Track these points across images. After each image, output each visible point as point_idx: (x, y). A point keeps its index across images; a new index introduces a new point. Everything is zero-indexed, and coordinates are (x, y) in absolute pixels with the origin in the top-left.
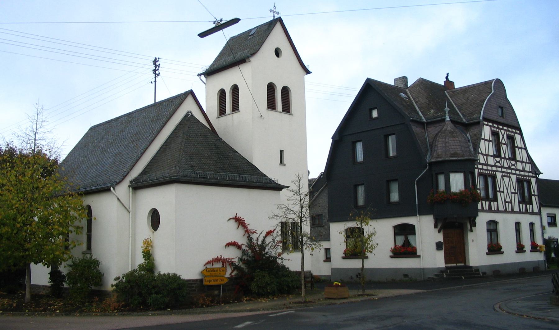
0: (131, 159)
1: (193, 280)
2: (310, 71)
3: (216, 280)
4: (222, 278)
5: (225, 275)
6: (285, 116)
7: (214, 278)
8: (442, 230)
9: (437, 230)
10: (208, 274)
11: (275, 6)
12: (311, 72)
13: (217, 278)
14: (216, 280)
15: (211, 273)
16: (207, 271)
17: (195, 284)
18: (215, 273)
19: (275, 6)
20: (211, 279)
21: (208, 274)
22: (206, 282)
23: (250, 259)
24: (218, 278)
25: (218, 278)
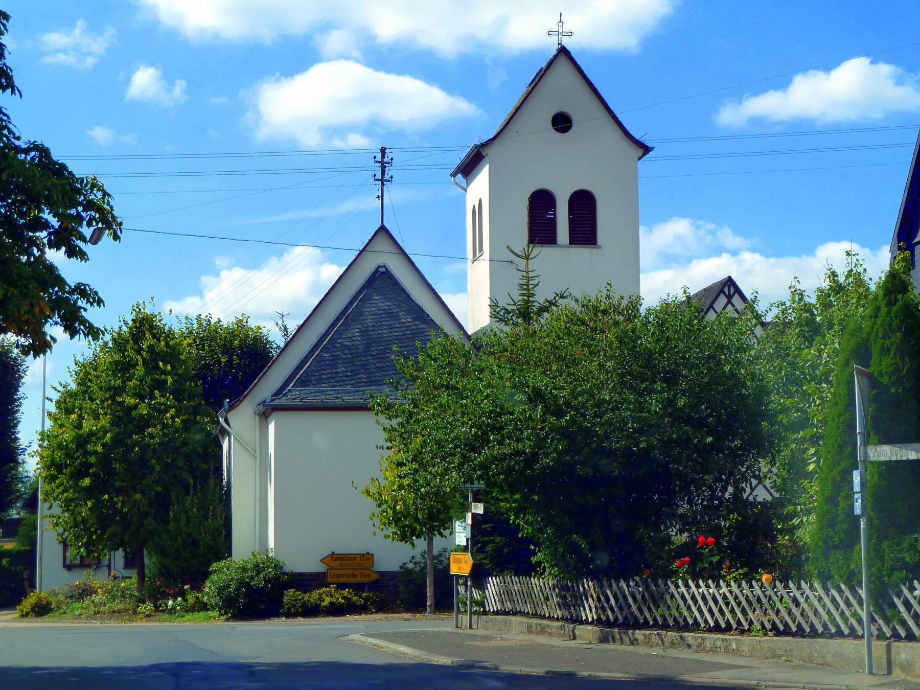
0: (335, 384)
1: (311, 574)
2: (650, 145)
3: (353, 575)
4: (367, 572)
5: (372, 567)
6: (582, 253)
7: (349, 572)
8: (32, 352)
9: (193, 316)
10: (336, 564)
11: (561, 21)
12: (652, 148)
13: (355, 572)
14: (353, 575)
15: (341, 564)
16: (332, 558)
17: (315, 580)
18: (350, 562)
19: (561, 21)
20: (342, 572)
21: (336, 564)
22: (331, 577)
23: (511, 522)
24: (358, 572)
25: (358, 572)
